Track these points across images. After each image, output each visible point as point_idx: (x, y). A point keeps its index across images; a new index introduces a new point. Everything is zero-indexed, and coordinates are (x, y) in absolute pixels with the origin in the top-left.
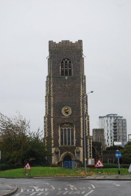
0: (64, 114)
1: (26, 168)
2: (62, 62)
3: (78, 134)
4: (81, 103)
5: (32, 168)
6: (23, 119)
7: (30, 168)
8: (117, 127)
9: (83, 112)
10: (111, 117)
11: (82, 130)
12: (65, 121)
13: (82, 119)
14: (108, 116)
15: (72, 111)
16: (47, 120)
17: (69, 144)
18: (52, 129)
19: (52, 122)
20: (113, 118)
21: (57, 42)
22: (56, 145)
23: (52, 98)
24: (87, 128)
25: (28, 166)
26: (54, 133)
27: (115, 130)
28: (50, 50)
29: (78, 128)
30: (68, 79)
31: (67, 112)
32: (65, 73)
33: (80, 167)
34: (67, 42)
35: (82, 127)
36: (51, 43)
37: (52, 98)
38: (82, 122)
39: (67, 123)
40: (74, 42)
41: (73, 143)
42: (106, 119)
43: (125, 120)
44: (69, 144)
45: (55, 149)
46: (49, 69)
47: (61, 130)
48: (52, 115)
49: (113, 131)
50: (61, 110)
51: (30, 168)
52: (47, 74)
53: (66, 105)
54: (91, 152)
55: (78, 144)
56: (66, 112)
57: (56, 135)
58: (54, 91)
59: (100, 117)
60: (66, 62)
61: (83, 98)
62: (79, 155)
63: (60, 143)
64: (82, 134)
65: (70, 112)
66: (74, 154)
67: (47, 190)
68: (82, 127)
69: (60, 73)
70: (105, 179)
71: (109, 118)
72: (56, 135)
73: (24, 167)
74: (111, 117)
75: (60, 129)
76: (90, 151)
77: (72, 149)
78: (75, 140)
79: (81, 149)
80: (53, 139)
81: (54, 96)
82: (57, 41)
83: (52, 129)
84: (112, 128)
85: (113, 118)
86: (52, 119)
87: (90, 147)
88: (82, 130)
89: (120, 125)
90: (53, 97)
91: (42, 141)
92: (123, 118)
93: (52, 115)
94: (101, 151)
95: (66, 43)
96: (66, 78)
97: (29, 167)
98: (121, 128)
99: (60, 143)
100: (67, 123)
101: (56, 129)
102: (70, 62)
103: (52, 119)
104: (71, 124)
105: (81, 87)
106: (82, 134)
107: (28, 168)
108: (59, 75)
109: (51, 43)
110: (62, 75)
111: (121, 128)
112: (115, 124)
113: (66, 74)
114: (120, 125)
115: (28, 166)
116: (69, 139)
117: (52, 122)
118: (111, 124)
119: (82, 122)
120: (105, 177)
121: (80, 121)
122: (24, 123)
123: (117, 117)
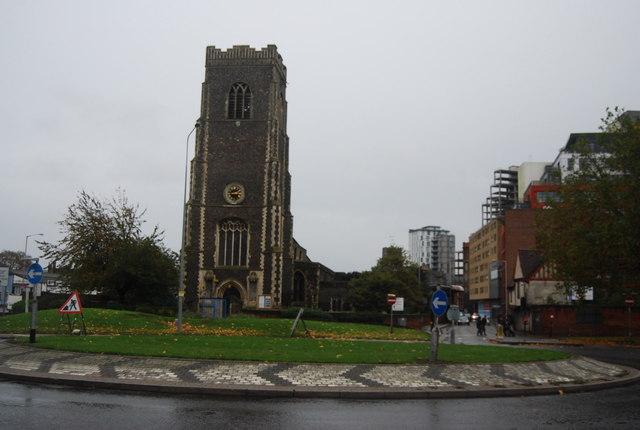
0: (230, 201)
1: (66, 308)
2: (232, 91)
3: (256, 242)
4: (266, 177)
5: (89, 310)
6: (128, 206)
7: (78, 310)
8: (439, 249)
9: (269, 195)
10: (429, 232)
11: (264, 235)
12: (231, 214)
13: (265, 210)
14: (424, 229)
15: (246, 194)
16: (191, 211)
17: (236, 262)
18: (202, 230)
19: (202, 215)
20: (432, 234)
21: (224, 50)
22: (209, 263)
23: (205, 166)
24: (274, 229)
25: (73, 303)
26: (206, 239)
27: (435, 253)
28: (208, 65)
29: (257, 229)
30: (242, 127)
31: (234, 195)
32: (236, 112)
33: (237, 312)
34: (244, 49)
35: (264, 228)
36: (211, 50)
37: (205, 166)
38: (264, 217)
39: (234, 219)
40: (258, 49)
41: (244, 263)
42: (420, 233)
43: (453, 236)
44: (236, 262)
45: (205, 272)
46: (204, 103)
47: (222, 233)
48: (203, 202)
49: (431, 255)
50: (222, 191)
51: (78, 310)
52: (198, 115)
53: (234, 181)
54: (280, 282)
55: (255, 265)
56: (232, 196)
57: (209, 242)
58: (210, 151)
59: (411, 231)
60: (240, 91)
61: (270, 165)
62: (256, 288)
63: (216, 260)
64: (263, 243)
65: (242, 195)
66: (245, 285)
67: (591, 298)
68: (264, 228)
69: (226, 115)
70: (44, 375)
71: (426, 233)
72: (209, 242)
73: (59, 307)
74: (429, 232)
75: (218, 230)
76: (277, 279)
77: (241, 275)
78: (248, 255)
79: (260, 275)
80: (264, 254)
81: (210, 162)
82: (224, 46)
83: (202, 230)
84: (430, 249)
85: (432, 234)
86: (203, 209)
87: (278, 272)
88: (264, 235)
89: (444, 244)
90: (208, 164)
91: (431, 266)
92: (449, 234)
93: (203, 202)
94: (316, 281)
95: (242, 51)
96: (238, 123)
97: (77, 305)
98: (445, 250)
99: (216, 260)
100: (234, 219)
101: (210, 231)
102: (248, 91)
103: (203, 209)
104: (243, 222)
105: (268, 143)
106: (263, 243)
107: (73, 309)
108: (223, 117)
109: (211, 50)
110: (231, 116)
111: (445, 250)
112: (435, 242)
113: (239, 116)
114: (444, 244)
115: (73, 303)
116: (236, 252)
117: (202, 215)
118: (428, 243)
119: (264, 217)
120: (45, 367)
121: (261, 214)
122: (129, 212)
123: (440, 231)
